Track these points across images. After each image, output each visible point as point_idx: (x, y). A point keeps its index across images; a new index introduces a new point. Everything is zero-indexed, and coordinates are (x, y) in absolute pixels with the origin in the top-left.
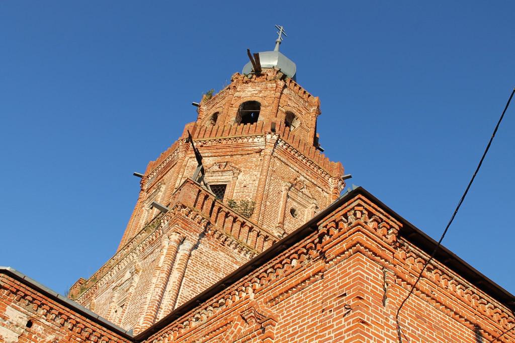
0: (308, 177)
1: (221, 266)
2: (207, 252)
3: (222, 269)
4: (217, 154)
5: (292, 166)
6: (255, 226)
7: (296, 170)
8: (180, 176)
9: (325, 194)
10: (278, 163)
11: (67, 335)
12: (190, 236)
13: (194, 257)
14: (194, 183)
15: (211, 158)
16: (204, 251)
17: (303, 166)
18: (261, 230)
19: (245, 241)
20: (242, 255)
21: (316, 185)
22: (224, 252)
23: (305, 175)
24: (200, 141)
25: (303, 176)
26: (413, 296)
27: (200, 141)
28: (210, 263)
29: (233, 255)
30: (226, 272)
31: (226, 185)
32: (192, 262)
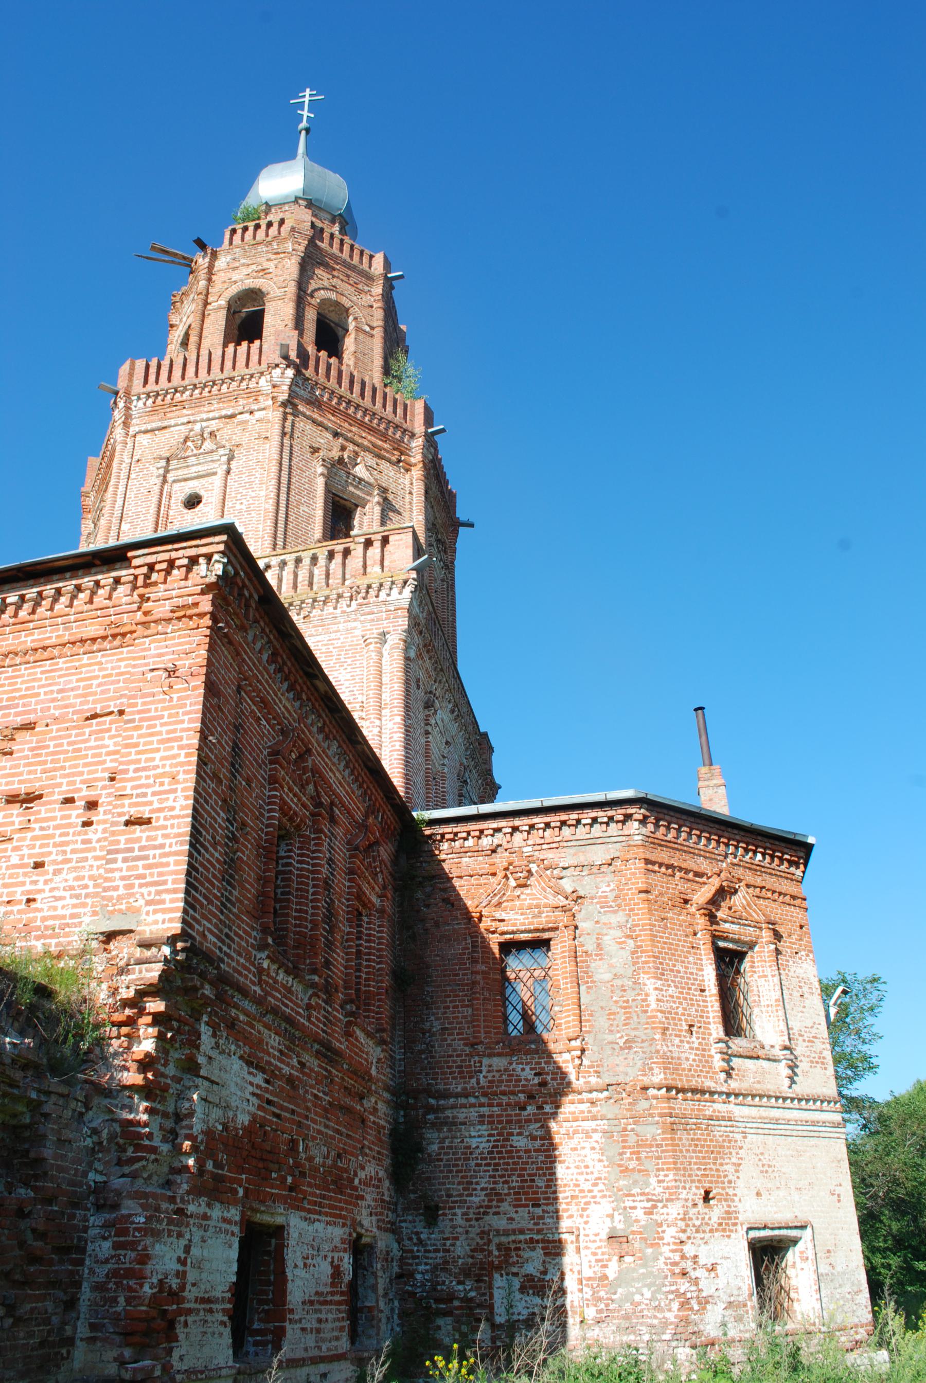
0: (211, 415)
5: (172, 422)
7: (183, 424)
9: (258, 415)
21: (233, 416)
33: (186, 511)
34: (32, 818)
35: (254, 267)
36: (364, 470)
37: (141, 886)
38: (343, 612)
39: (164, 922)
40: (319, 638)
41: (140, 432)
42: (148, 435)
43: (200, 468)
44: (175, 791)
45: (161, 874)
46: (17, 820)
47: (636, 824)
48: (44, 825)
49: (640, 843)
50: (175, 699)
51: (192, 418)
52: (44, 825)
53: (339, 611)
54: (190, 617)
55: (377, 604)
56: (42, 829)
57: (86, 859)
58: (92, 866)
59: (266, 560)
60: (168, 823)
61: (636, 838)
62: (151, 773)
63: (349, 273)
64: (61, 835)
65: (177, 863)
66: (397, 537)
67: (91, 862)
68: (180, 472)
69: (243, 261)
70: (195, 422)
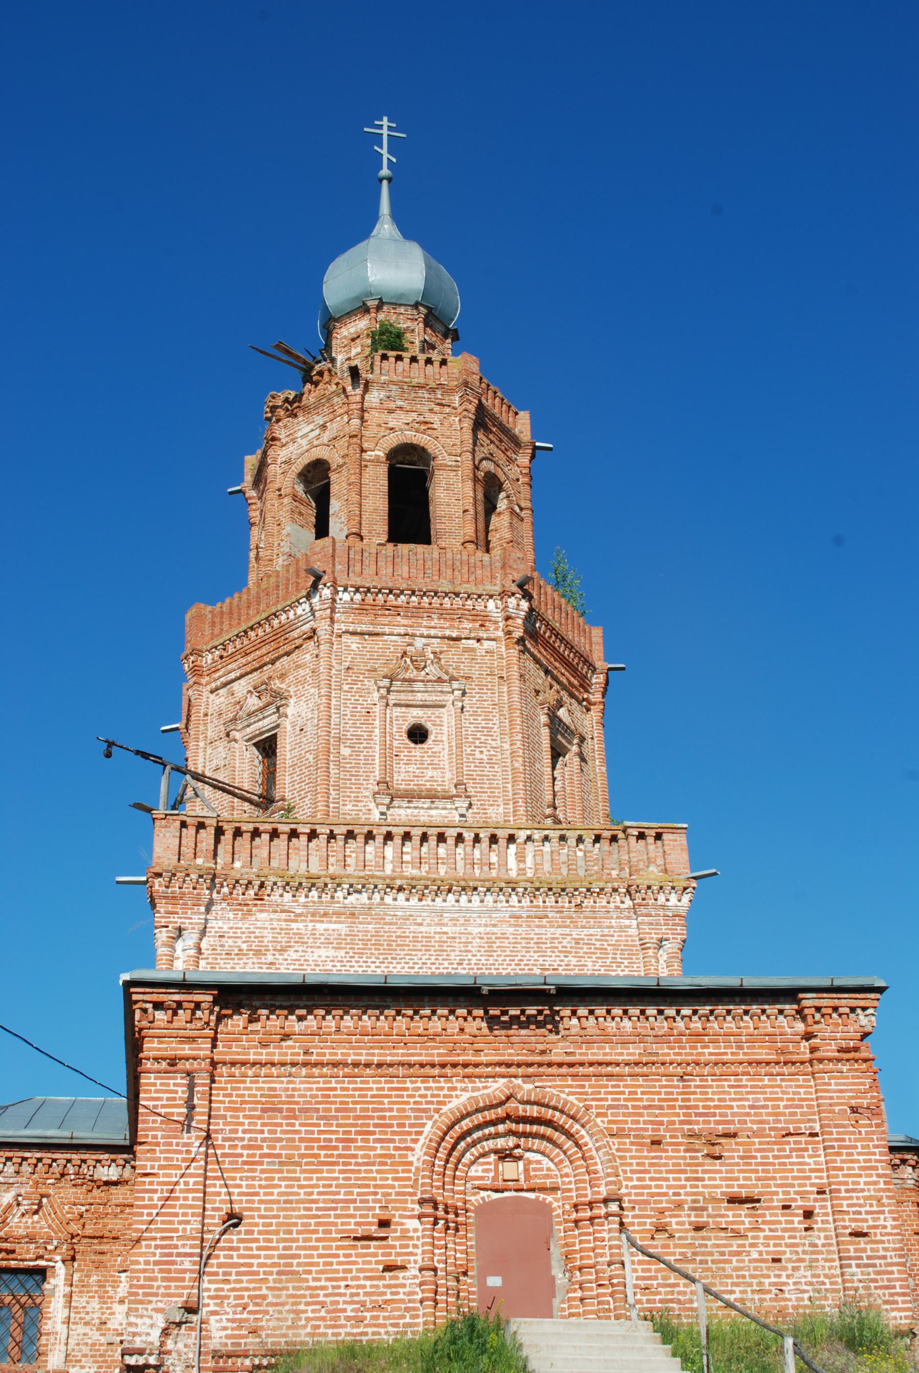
0: (433, 632)
1: (266, 940)
2: (231, 928)
3: (270, 945)
4: (248, 668)
5: (387, 630)
6: (317, 827)
7: (400, 635)
8: (202, 744)
9: (487, 644)
10: (354, 643)
11: (31, 1183)
12: (187, 921)
13: (210, 952)
14: (166, 815)
15: (242, 681)
16: (226, 929)
17: (416, 613)
18: (333, 827)
19: (304, 866)
20: (302, 899)
21: (457, 639)
22: (267, 911)
23: (425, 632)
24: (216, 647)
25: (422, 636)
26: (221, 1082)
27: (216, 647)
28: (244, 946)
29: (286, 908)
30: (279, 948)
31: (276, 734)
32: (207, 963)
33: (405, 736)
34: (760, 1220)
35: (414, 415)
36: (567, 714)
37: (876, 1288)
38: (617, 907)
39: (901, 1319)
40: (592, 931)
41: (347, 632)
42: (356, 638)
43: (426, 696)
44: (883, 1212)
45: (889, 1280)
46: (747, 1220)
47: (910, 1169)
48: (773, 1227)
49: (912, 1186)
50: (863, 1133)
51: (410, 631)
52: (773, 1227)
53: (612, 905)
54: (856, 1061)
55: (655, 907)
56: (771, 1230)
57: (817, 1260)
58: (823, 1266)
59: (528, 832)
60: (885, 1238)
61: (909, 1182)
62: (860, 1195)
63: (502, 437)
64: (790, 1237)
65: (183, 1092)
66: (670, 836)
67: (821, 1263)
68: (402, 696)
69: (400, 403)
70: (414, 635)
